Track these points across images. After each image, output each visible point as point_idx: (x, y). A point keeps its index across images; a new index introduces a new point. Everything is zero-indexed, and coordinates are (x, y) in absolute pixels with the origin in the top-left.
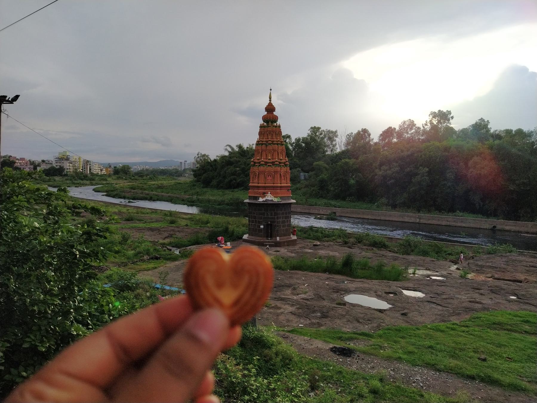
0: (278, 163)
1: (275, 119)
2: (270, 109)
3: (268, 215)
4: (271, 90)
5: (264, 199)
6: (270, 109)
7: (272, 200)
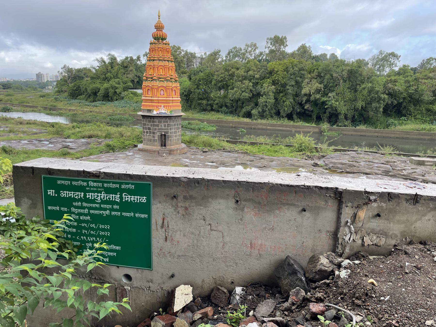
3: (161, 126)
6: (159, 27)
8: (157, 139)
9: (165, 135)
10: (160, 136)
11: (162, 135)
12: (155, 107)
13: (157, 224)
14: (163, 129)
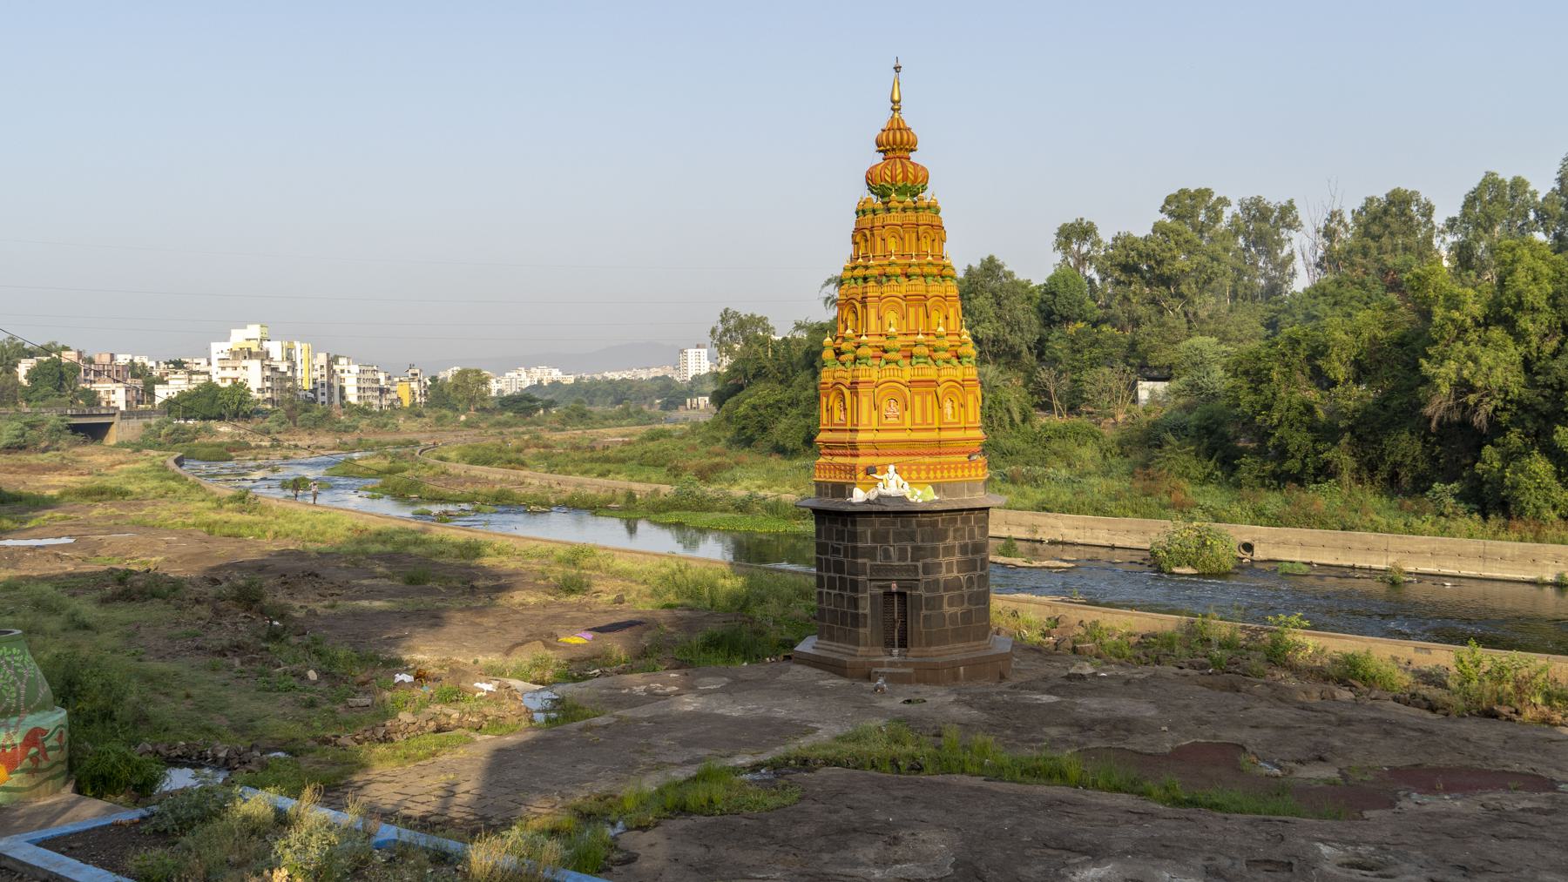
0: (926, 351)
1: (914, 186)
2: (895, 144)
3: (887, 556)
4: (898, 69)
5: (873, 495)
6: (895, 144)
7: (903, 499)
8: (868, 611)
9: (902, 595)
10: (880, 600)
11: (889, 594)
12: (861, 476)
13: (1192, 803)
14: (893, 569)
